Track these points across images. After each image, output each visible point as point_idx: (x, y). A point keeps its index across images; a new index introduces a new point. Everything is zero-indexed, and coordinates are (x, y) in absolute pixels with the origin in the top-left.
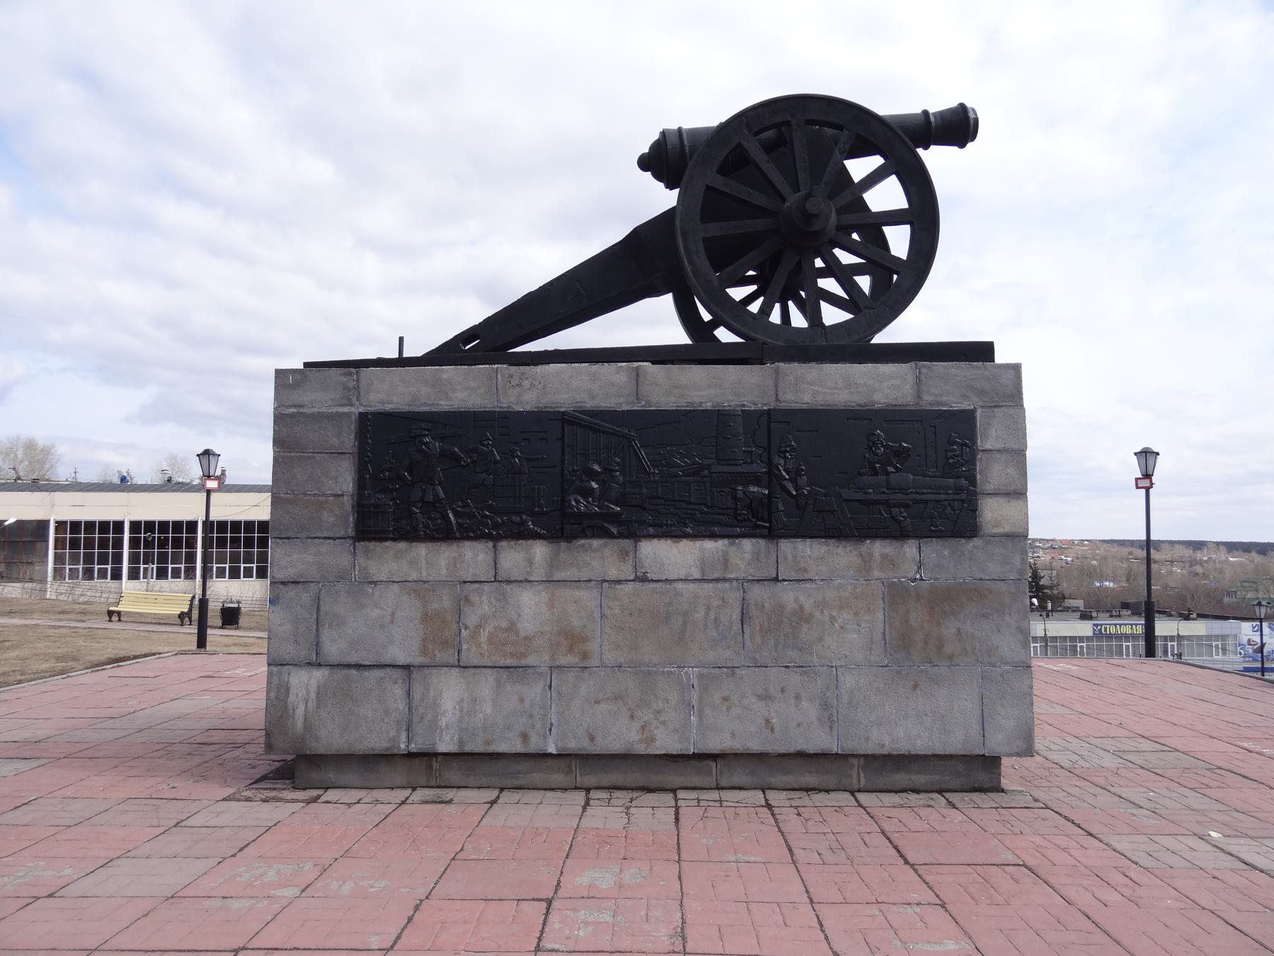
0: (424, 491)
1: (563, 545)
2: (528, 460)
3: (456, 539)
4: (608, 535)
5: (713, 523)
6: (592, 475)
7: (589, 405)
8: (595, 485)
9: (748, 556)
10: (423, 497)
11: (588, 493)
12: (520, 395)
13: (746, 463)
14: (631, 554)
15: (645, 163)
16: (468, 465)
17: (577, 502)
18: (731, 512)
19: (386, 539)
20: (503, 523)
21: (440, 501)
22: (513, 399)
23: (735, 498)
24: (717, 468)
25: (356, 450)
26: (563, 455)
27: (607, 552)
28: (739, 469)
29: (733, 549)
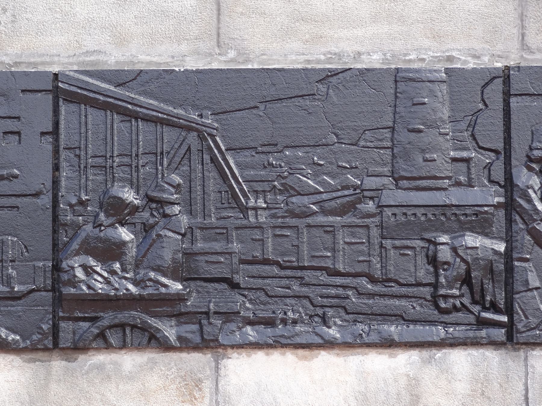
1: (58, 364)
4: (155, 341)
5: (387, 316)
6: (119, 211)
7: (114, 58)
8: (125, 234)
9: (462, 387)
11: (110, 252)
13: (458, 184)
14: (207, 385)
17: (88, 270)
18: (426, 291)
23: (433, 260)
24: (394, 196)
26: (56, 168)
27: (153, 381)
28: (439, 198)
29: (429, 374)
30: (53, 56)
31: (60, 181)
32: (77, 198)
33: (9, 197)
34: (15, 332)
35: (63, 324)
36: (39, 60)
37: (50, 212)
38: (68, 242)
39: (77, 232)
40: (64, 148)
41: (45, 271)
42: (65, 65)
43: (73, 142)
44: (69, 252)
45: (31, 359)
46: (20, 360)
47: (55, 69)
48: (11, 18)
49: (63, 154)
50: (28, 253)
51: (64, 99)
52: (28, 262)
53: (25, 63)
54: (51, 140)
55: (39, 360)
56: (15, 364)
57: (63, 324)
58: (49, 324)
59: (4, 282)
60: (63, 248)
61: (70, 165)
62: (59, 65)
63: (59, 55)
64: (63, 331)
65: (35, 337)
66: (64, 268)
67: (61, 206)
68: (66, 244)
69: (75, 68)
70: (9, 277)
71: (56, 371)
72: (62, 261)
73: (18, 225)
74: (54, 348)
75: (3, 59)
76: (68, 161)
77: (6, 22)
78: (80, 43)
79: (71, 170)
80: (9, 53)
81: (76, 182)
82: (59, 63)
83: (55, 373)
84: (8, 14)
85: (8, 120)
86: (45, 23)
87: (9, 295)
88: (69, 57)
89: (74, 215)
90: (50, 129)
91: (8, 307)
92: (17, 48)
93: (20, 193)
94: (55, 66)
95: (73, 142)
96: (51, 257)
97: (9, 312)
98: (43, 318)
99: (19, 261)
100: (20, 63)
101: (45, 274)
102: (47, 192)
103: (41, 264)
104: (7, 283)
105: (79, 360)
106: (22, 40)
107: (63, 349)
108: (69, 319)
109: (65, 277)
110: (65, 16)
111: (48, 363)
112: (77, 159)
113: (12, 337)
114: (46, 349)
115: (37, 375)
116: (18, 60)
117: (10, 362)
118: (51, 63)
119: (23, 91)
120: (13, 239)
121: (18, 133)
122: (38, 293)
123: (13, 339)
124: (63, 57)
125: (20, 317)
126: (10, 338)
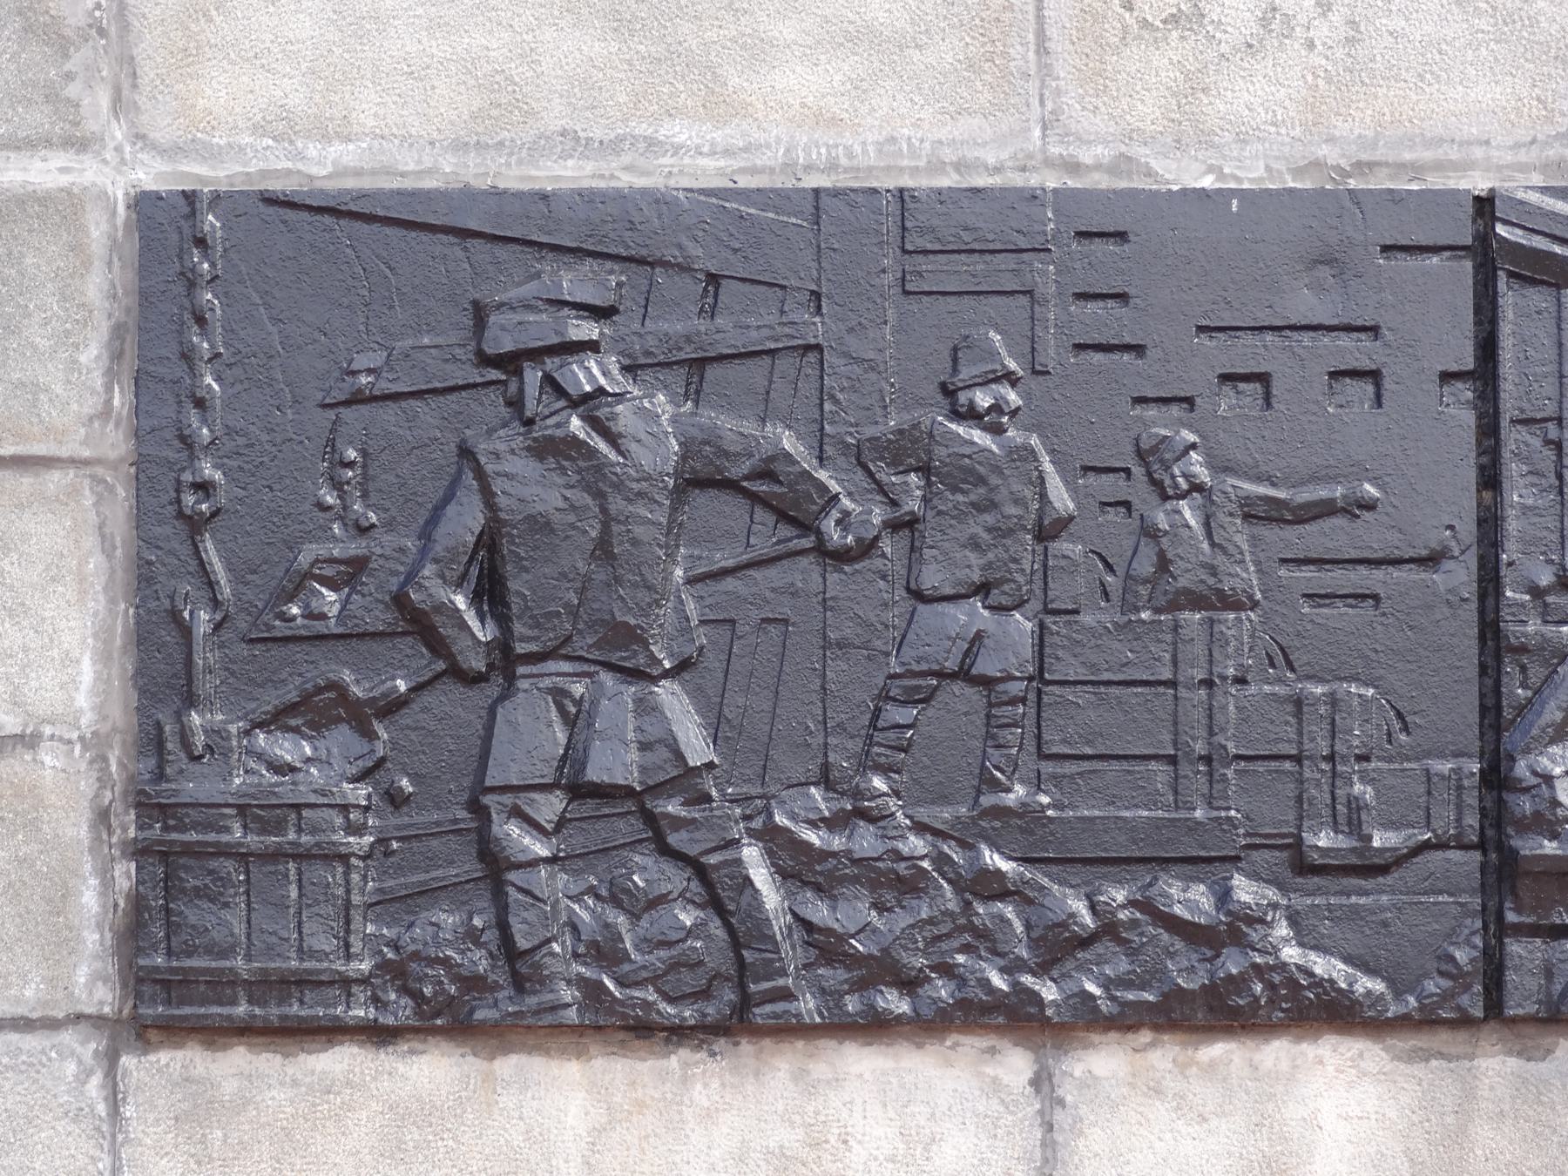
0: (576, 718)
1: (1495, 1067)
2: (1257, 513)
3: (792, 1030)
10: (574, 757)
12: (1195, 85)
15: (203, 961)
16: (867, 548)
19: (331, 1032)
20: (1109, 929)
21: (686, 780)
22: (1147, 112)
25: (116, 443)
26: (1490, 479)
30: (1469, 143)
31: (1503, 519)
32: (1554, 569)
33: (1350, 566)
34: (1370, 971)
35: (1515, 948)
36: (1427, 155)
37: (1470, 613)
38: (1530, 701)
39: (1555, 671)
40: (1512, 421)
41: (1460, 788)
42: (1507, 173)
43: (1540, 403)
44: (1534, 732)
45: (1414, 1050)
46: (1383, 1054)
47: (1480, 184)
48: (1344, 31)
49: (1513, 438)
50: (1409, 734)
51: (1511, 275)
52: (1408, 760)
53: (1387, 164)
54: (1470, 395)
55: (1448, 1058)
56: (1370, 1065)
57: (1515, 948)
58: (1475, 947)
59: (1341, 820)
60: (1514, 720)
61: (1530, 472)
62: (1487, 170)
63: (1487, 142)
64: (1516, 969)
65: (1431, 986)
66: (1520, 781)
67: (1509, 594)
68: (1522, 709)
69: (1537, 180)
70: (1356, 806)
71: (1492, 1088)
72: (1513, 759)
73: (1376, 651)
74: (1486, 1019)
75: (1320, 153)
76: (1526, 460)
77: (1330, 43)
78: (1550, 106)
79: (1533, 485)
80: (1337, 133)
81: (1552, 523)
82: (1488, 167)
83: (1486, 1094)
84: (1335, 17)
85: (1342, 334)
86: (1444, 47)
87: (1354, 860)
88: (1517, 146)
89: (1546, 622)
90: (1469, 364)
91: (1349, 896)
92: (1362, 120)
93: (1380, 555)
94: (1477, 174)
95: (1540, 403)
96: (1476, 746)
97: (1355, 909)
98: (1453, 929)
99: (1380, 759)
100: (1372, 165)
101: (1459, 796)
102: (1463, 552)
103: (1446, 767)
104: (1349, 823)
105: (1558, 1053)
106: (1376, 97)
107: (1514, 1020)
108: (1534, 931)
109: (1526, 805)
110: (1506, 24)
111: (1467, 1064)
112: (1550, 454)
113: (1367, 984)
114: (1464, 1022)
115: (1434, 1098)
116: (1364, 157)
117: (1352, 1059)
118: (1465, 166)
119: (1386, 249)
120: (1362, 691)
121: (1374, 375)
122: (1439, 854)
123: (1369, 993)
124: (1498, 148)
125: (1385, 924)
126: (1359, 989)
